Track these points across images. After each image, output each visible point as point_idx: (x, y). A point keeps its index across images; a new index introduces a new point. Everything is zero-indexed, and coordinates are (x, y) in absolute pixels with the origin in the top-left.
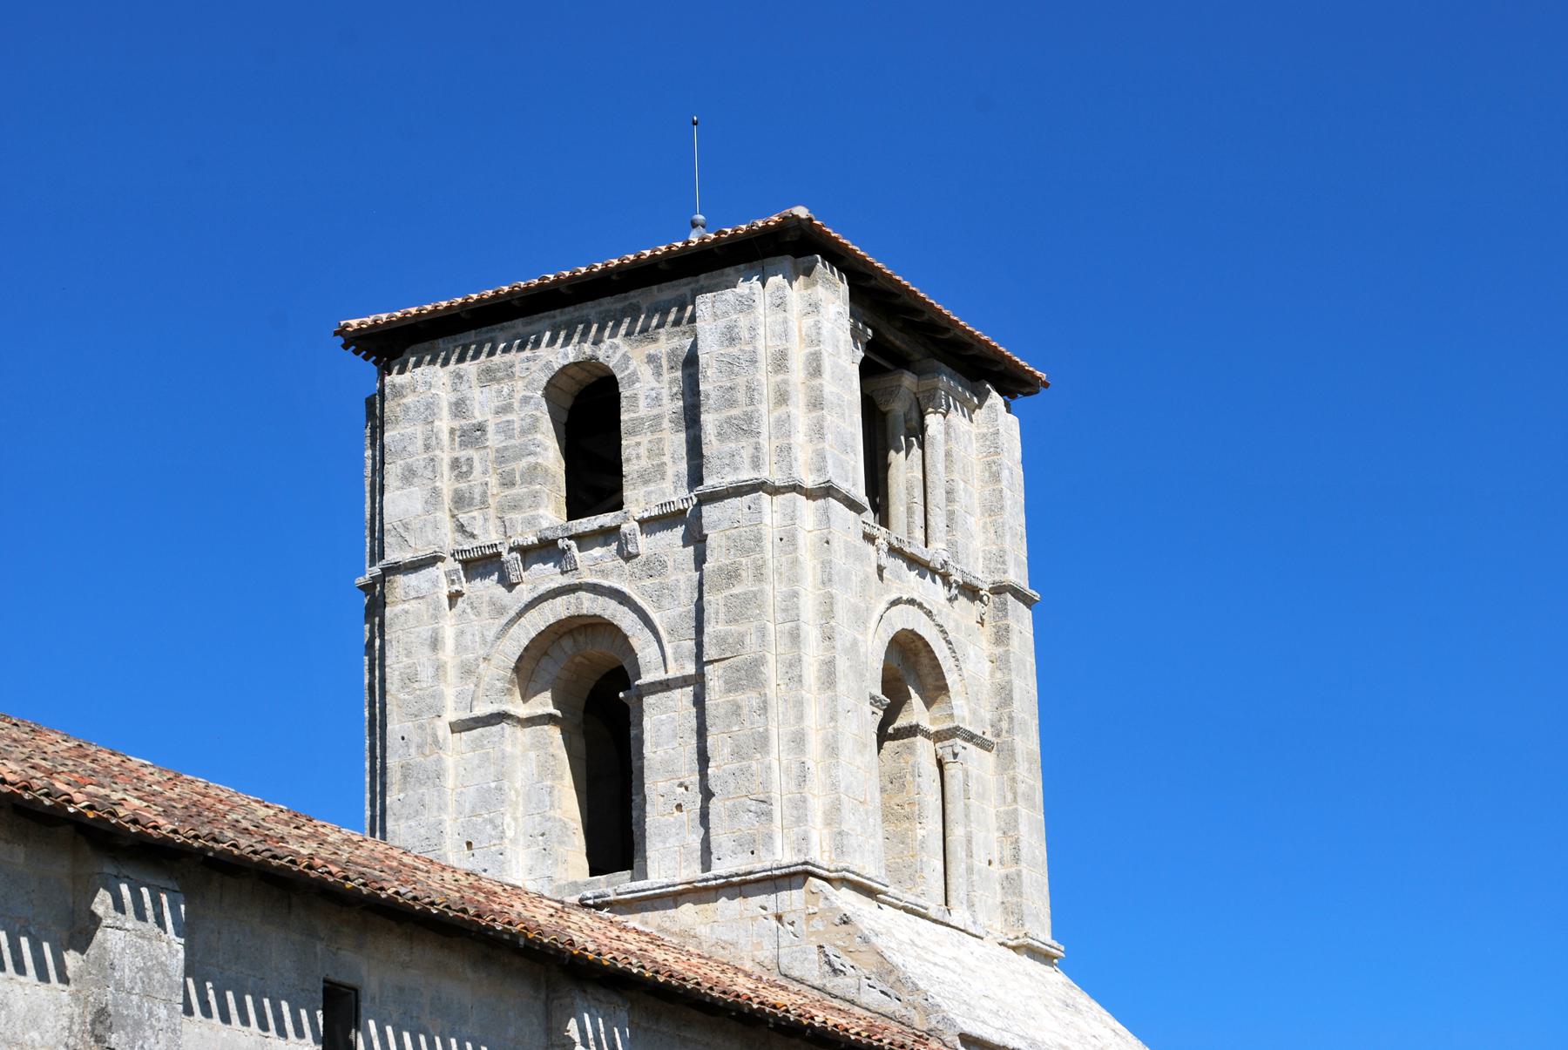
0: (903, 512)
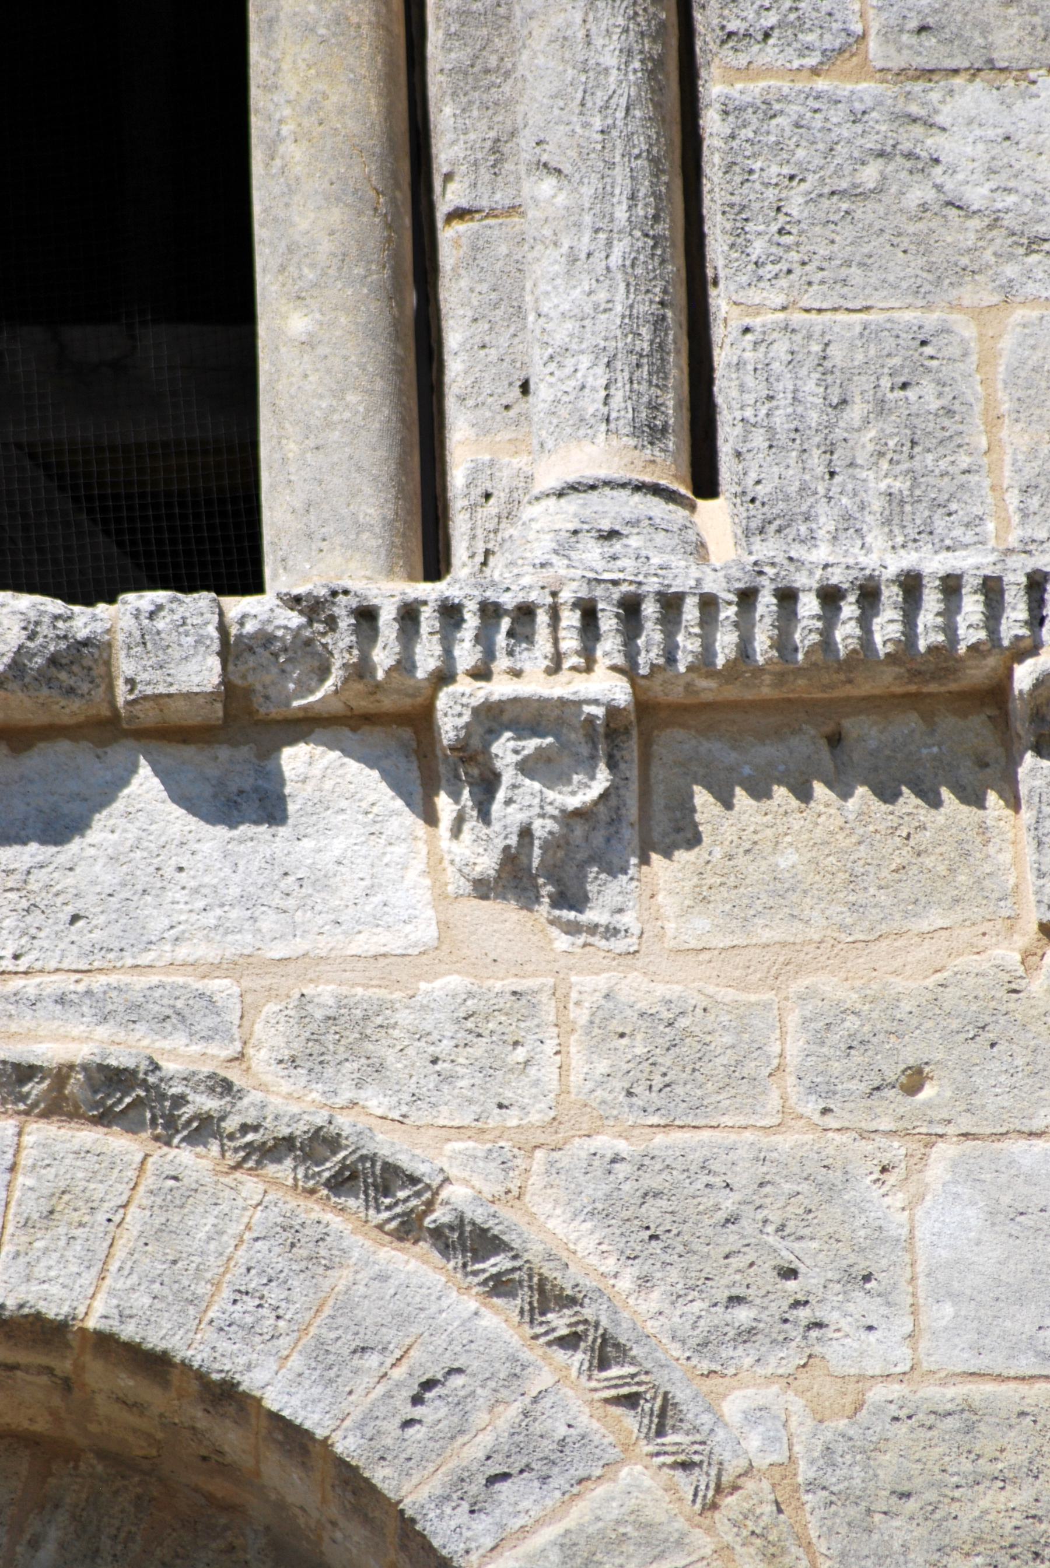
0: (308, 344)
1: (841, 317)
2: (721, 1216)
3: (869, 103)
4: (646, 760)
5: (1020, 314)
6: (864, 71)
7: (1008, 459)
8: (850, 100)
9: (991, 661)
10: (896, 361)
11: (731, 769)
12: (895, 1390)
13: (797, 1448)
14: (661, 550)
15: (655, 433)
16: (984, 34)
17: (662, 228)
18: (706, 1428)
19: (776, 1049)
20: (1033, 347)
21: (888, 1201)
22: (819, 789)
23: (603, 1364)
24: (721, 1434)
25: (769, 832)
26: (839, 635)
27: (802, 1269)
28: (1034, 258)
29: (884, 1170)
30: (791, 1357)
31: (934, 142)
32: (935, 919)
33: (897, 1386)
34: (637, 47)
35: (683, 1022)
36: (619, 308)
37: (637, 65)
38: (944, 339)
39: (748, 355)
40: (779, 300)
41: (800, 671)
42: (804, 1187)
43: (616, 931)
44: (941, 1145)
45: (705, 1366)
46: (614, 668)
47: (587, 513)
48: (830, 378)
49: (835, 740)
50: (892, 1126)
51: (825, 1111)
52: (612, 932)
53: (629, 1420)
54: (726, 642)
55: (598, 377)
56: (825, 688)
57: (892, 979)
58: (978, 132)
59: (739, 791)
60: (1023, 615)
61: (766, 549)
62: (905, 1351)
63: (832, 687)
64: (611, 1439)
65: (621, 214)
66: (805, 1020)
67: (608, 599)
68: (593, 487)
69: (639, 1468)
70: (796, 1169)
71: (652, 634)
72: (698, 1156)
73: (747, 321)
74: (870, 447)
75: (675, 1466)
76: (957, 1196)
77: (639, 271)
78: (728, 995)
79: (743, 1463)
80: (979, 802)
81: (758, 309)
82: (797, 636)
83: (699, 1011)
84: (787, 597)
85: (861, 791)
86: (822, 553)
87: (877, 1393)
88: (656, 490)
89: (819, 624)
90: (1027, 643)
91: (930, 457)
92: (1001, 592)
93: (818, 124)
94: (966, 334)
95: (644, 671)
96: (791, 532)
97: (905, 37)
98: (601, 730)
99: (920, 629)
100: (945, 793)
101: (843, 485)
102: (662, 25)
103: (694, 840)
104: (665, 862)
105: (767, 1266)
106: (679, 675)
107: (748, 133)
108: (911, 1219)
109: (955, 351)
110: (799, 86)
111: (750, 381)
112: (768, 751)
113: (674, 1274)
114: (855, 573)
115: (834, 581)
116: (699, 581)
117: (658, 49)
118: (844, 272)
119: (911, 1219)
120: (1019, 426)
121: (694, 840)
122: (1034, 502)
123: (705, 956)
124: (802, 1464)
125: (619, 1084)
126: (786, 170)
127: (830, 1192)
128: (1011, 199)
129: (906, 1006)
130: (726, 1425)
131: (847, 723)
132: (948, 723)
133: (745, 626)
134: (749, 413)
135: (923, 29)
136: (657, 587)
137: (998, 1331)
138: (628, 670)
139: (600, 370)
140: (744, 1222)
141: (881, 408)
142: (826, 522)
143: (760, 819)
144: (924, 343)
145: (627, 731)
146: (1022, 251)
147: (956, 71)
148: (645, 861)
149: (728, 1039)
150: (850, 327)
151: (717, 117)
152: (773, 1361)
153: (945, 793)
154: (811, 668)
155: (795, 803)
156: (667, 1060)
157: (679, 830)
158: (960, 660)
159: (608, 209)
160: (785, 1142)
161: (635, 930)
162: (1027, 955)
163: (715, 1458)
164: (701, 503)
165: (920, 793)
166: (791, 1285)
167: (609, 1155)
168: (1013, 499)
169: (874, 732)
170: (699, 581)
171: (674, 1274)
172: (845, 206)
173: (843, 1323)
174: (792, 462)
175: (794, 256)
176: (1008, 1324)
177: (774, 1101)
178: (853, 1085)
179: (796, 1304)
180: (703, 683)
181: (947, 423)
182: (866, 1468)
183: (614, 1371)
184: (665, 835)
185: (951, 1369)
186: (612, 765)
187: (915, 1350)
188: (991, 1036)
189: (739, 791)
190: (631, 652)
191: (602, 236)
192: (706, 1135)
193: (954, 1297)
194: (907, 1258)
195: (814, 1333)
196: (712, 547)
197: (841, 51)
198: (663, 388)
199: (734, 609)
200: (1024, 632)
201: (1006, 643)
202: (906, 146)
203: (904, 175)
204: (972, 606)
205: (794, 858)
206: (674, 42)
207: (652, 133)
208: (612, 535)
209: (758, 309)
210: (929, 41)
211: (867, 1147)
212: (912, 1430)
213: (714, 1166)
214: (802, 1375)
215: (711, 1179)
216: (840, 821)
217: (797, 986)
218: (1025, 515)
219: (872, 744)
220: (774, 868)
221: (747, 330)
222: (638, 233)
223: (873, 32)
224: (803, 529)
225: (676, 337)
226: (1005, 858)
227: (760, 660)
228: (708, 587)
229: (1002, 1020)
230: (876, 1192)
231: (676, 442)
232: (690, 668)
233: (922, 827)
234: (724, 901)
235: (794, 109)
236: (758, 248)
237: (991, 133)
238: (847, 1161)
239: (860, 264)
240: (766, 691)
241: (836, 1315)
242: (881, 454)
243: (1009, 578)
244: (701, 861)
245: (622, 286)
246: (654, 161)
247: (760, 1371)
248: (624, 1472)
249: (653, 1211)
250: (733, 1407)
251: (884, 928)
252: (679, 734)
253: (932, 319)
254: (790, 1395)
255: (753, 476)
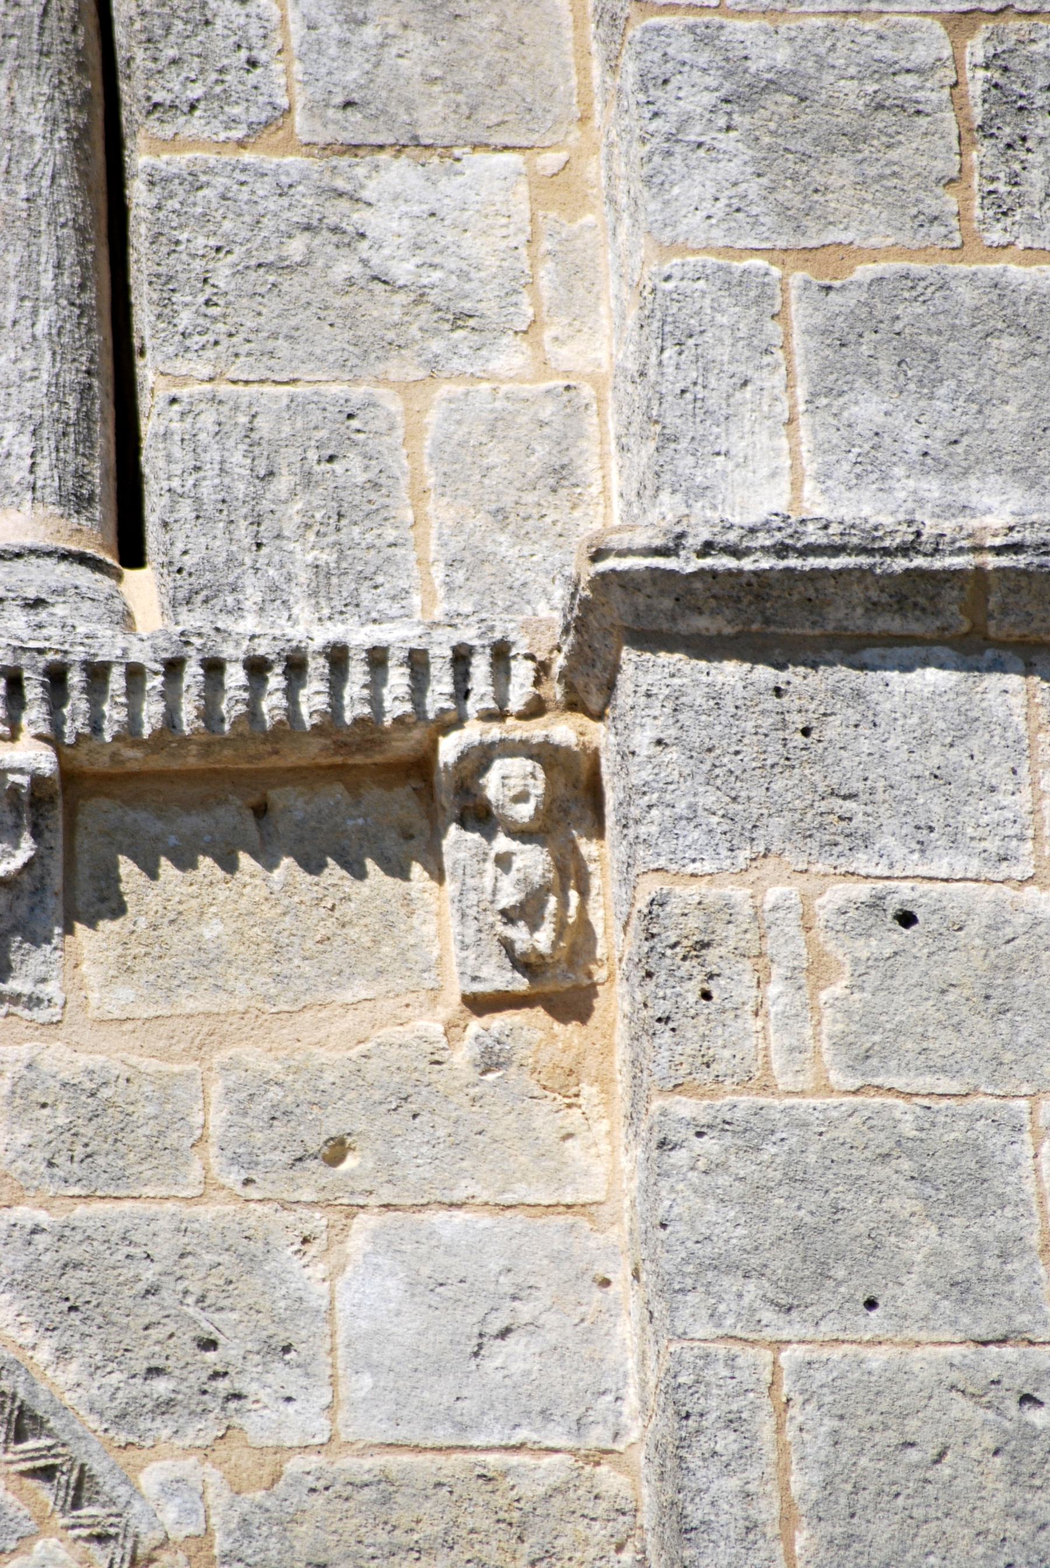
1: (268, 389)
2: (141, 1287)
3: (295, 176)
4: (70, 829)
5: (445, 389)
6: (290, 145)
7: (434, 533)
8: (276, 174)
9: (417, 734)
10: (323, 434)
11: (157, 839)
12: (313, 1461)
13: (213, 1520)
14: (87, 619)
15: (81, 502)
16: (409, 110)
17: (88, 297)
18: (122, 1500)
19: (198, 1119)
20: (459, 422)
21: (308, 1271)
22: (245, 860)
23: (20, 1437)
24: (137, 1506)
25: (194, 903)
26: (265, 706)
27: (222, 1340)
28: (459, 334)
29: (305, 1241)
30: (209, 1429)
31: (359, 217)
32: (359, 990)
33: (314, 1458)
34: (62, 116)
35: (105, 1093)
36: (45, 377)
37: (62, 133)
38: (370, 413)
39: (175, 426)
40: (206, 371)
41: (226, 742)
42: (225, 1258)
43: (39, 1001)
44: (362, 1216)
45: (123, 1438)
46: (39, 737)
47: (12, 581)
48: (257, 450)
49: (261, 811)
50: (314, 1197)
51: (248, 1182)
52: (34, 1002)
53: (45, 1493)
54: (152, 712)
55: (24, 445)
56: (251, 759)
57: (315, 1050)
58: (404, 208)
59: (164, 861)
60: (449, 688)
61: (193, 619)
62: (324, 1422)
63: (258, 757)
64: (26, 1511)
65: (47, 282)
66: (229, 1091)
67: (33, 668)
68: (19, 555)
69: (54, 1541)
70: (217, 1240)
71: (77, 703)
72: (118, 1227)
73: (174, 392)
74: (297, 519)
75: (90, 1538)
76: (377, 1267)
77: (65, 339)
78: (152, 1065)
79: (159, 1535)
80: (403, 874)
81: (184, 380)
82: (224, 707)
83: (122, 1082)
84: (214, 667)
85: (287, 861)
86: (249, 624)
87: (295, 1465)
88: (83, 559)
89: (246, 695)
90: (452, 716)
91: (356, 530)
92: (426, 665)
93: (244, 196)
94: (393, 408)
95: (69, 740)
96: (218, 603)
97: (331, 113)
98: (26, 799)
99: (346, 701)
100: (370, 865)
101: (270, 556)
102: (88, 94)
103: (119, 910)
104: (90, 932)
105: (186, 1337)
106: (104, 745)
107: (174, 204)
108: (332, 1290)
109: (381, 425)
110: (225, 158)
111: (177, 451)
112: (193, 822)
113: (93, 1346)
114: (281, 644)
115: (261, 652)
116: (125, 651)
117: (82, 119)
118: (271, 344)
119: (332, 1290)
120: (446, 500)
121: (119, 910)
122: (460, 576)
123: (128, 1026)
124: (218, 1537)
125: (40, 1155)
126: (213, 242)
127: (251, 1263)
128: (436, 275)
129: (329, 1077)
130: (142, 1497)
131: (273, 795)
132: (373, 794)
133: (171, 695)
134: (175, 483)
135: (348, 104)
136: (83, 656)
137: (415, 1402)
138: (54, 739)
139: (26, 438)
140: (164, 1293)
141: (308, 480)
142: (253, 593)
143: (185, 889)
144: (350, 416)
145: (52, 800)
146: (447, 326)
147: (381, 147)
148: (69, 930)
149: (151, 1110)
150: (277, 399)
151: (143, 187)
152: (191, 1432)
153: (370, 865)
154: (238, 738)
155: (220, 873)
156: (89, 1131)
157: (103, 900)
158: (386, 732)
159: (34, 277)
160: (206, 1213)
161: (58, 1000)
162: (449, 1027)
163: (131, 1530)
164: (128, 573)
165: (345, 865)
166: (210, 1356)
167: (29, 1226)
168: (438, 573)
169: (300, 803)
170: (125, 651)
171: (93, 1346)
172: (271, 279)
173: (263, 1395)
174: (219, 533)
175: (221, 327)
176: (426, 1394)
177: (196, 1171)
178: (276, 1156)
179: (215, 1375)
180: (129, 753)
181: (373, 496)
182: (282, 1539)
183: (31, 1444)
184: (90, 904)
185: (369, 1440)
186: (36, 835)
187: (333, 1421)
188: (414, 1107)
189: (164, 861)
190: (56, 721)
191: (28, 304)
192: (127, 1206)
193: (372, 1367)
194: (327, 1329)
195: (233, 1405)
196: (138, 617)
197: (267, 124)
198: (90, 457)
199: (161, 678)
200: (449, 705)
201: (431, 716)
202: (332, 220)
203: (330, 249)
204: (398, 679)
205: (219, 928)
206: (99, 111)
207: (78, 201)
208: (38, 603)
209: (184, 380)
210: (355, 116)
211: (288, 1217)
212: (329, 1501)
213: (135, 1237)
214: (220, 1447)
215: (132, 1250)
216: (265, 892)
217: (221, 1057)
218: (450, 588)
219: (298, 815)
220: (198, 938)
221: (174, 401)
222: (64, 302)
223: (298, 107)
224: (230, 600)
225: (102, 406)
226: (429, 930)
227: (187, 730)
228: (134, 657)
229: (425, 1091)
230: (297, 1263)
231: (102, 511)
232: (116, 738)
233: (347, 899)
234: (149, 971)
235: (220, 182)
236: (185, 319)
237: (416, 209)
238: (268, 1232)
239: (288, 337)
240: (192, 761)
241: (255, 1386)
242: (308, 526)
243: (434, 651)
244: (126, 931)
245: (48, 355)
246: (80, 230)
247: (178, 1442)
248: (40, 1543)
249: (72, 1282)
250: (149, 1479)
251: (307, 999)
252: (105, 803)
253: (359, 393)
254: (208, 1467)
255: (180, 546)
